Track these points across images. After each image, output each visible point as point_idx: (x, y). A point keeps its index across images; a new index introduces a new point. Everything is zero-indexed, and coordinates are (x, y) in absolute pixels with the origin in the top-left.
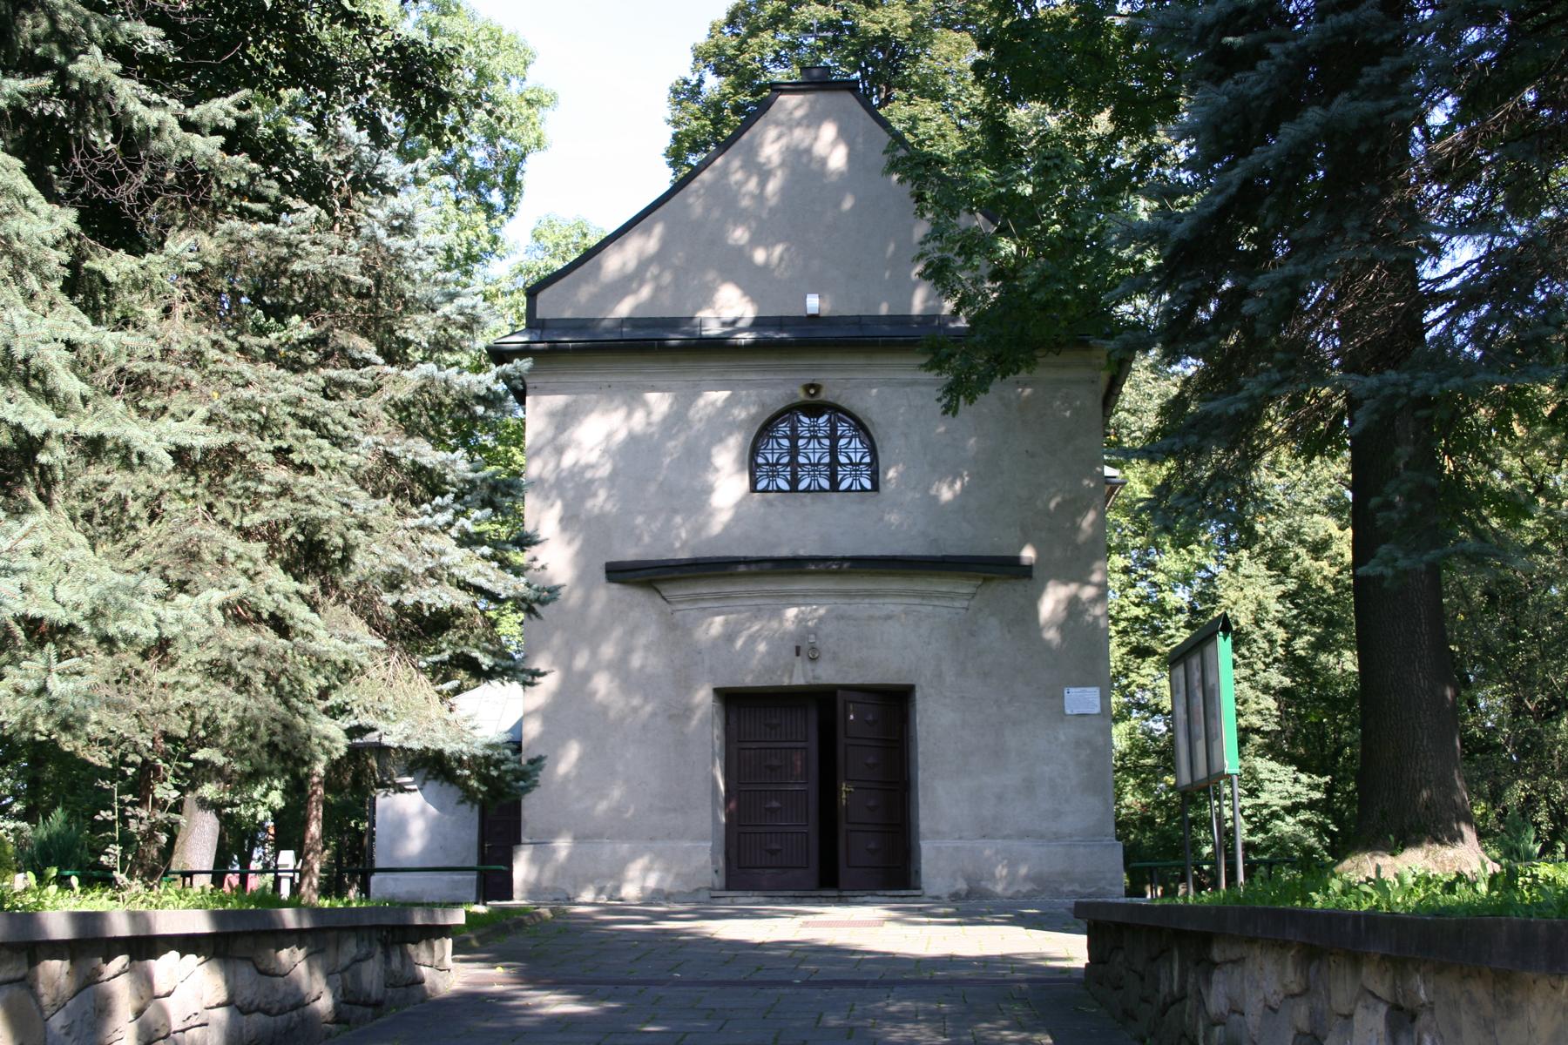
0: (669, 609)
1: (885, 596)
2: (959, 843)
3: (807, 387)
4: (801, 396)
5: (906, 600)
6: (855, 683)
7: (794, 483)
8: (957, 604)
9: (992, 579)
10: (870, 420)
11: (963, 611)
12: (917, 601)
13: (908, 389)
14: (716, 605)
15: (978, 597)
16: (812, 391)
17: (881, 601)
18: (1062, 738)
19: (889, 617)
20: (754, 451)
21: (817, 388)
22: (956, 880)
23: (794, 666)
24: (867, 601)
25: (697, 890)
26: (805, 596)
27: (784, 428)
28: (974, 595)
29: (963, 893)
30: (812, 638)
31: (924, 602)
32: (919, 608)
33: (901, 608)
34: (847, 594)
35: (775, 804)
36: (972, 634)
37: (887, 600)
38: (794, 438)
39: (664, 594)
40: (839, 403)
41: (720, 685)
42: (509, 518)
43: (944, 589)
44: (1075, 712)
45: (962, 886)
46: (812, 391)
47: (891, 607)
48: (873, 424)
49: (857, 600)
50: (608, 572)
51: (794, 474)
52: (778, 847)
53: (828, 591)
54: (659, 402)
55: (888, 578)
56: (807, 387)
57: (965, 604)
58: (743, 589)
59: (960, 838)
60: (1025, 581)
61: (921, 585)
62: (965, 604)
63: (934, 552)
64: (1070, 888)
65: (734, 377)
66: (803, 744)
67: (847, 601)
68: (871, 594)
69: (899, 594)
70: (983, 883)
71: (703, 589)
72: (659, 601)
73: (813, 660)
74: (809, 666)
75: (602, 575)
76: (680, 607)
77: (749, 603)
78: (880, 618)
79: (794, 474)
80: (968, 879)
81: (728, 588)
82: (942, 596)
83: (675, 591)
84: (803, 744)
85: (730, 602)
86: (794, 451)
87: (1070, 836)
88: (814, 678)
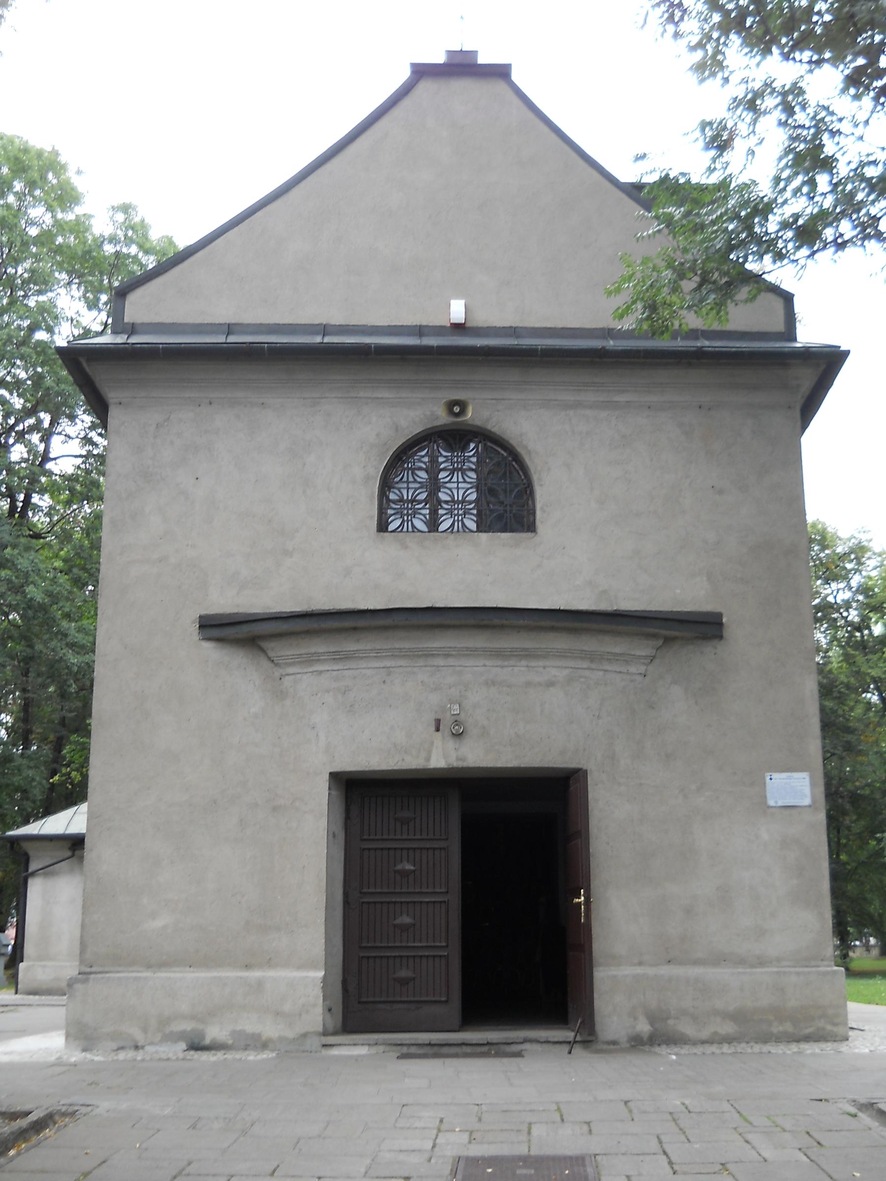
0: (277, 672)
1: (545, 657)
2: (639, 970)
3: (451, 405)
4: (442, 418)
5: (572, 663)
6: (510, 765)
7: (433, 525)
8: (633, 669)
9: (673, 639)
10: (525, 447)
11: (639, 678)
12: (585, 664)
13: (571, 413)
14: (336, 668)
15: (657, 661)
16: (457, 409)
17: (541, 663)
18: (765, 836)
19: (550, 684)
20: (386, 484)
21: (463, 405)
22: (636, 1019)
23: (432, 743)
24: (524, 663)
25: (305, 1035)
26: (447, 656)
27: (423, 457)
28: (652, 659)
29: (646, 1037)
30: (456, 709)
31: (593, 666)
32: (587, 673)
33: (566, 672)
34: (498, 654)
35: (406, 920)
36: (652, 706)
37: (548, 663)
38: (433, 470)
39: (271, 654)
40: (489, 427)
41: (338, 768)
42: (848, 822)
43: (617, 650)
44: (780, 804)
45: (644, 1027)
46: (457, 409)
47: (554, 672)
48: (529, 452)
49: (512, 662)
50: (201, 627)
51: (434, 512)
52: (410, 974)
53: (476, 649)
54: (877, 1124)
55: (649, 348)
56: (451, 405)
57: (642, 669)
58: (369, 647)
59: (640, 964)
60: (715, 642)
61: (590, 643)
62: (642, 669)
63: (604, 606)
64: (781, 1028)
65: (362, 394)
66: (442, 844)
67: (499, 663)
68: (528, 655)
69: (562, 655)
70: (671, 1022)
71: (319, 646)
72: (265, 663)
73: (458, 736)
74: (451, 744)
75: (194, 629)
76: (291, 670)
77: (377, 665)
78: (540, 684)
79: (434, 512)
80: (652, 1019)
81: (350, 645)
82: (615, 658)
83: (277, 649)
84: (442, 844)
85: (352, 664)
86: (434, 486)
87: (778, 960)
88: (458, 759)
